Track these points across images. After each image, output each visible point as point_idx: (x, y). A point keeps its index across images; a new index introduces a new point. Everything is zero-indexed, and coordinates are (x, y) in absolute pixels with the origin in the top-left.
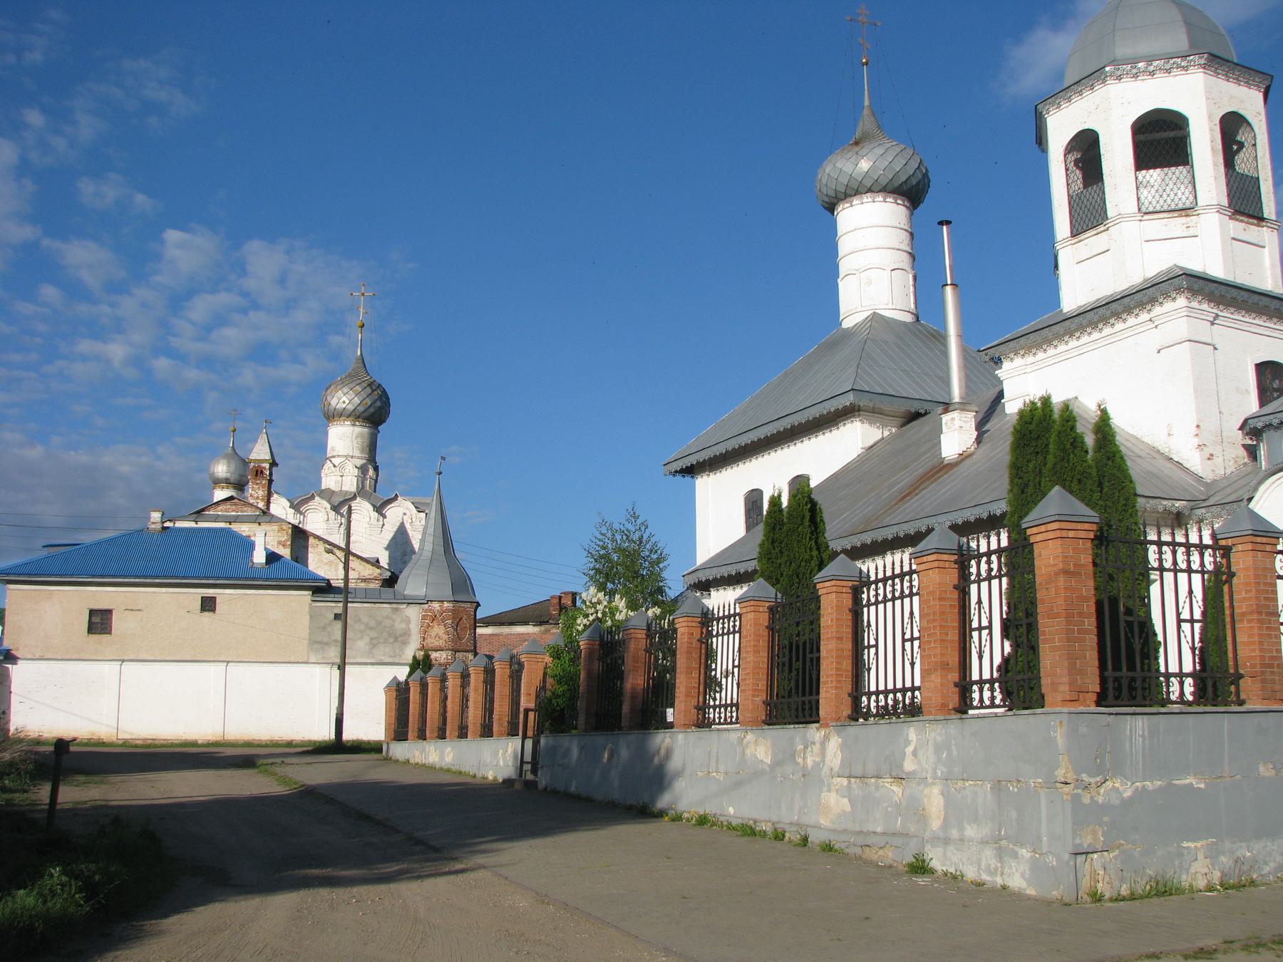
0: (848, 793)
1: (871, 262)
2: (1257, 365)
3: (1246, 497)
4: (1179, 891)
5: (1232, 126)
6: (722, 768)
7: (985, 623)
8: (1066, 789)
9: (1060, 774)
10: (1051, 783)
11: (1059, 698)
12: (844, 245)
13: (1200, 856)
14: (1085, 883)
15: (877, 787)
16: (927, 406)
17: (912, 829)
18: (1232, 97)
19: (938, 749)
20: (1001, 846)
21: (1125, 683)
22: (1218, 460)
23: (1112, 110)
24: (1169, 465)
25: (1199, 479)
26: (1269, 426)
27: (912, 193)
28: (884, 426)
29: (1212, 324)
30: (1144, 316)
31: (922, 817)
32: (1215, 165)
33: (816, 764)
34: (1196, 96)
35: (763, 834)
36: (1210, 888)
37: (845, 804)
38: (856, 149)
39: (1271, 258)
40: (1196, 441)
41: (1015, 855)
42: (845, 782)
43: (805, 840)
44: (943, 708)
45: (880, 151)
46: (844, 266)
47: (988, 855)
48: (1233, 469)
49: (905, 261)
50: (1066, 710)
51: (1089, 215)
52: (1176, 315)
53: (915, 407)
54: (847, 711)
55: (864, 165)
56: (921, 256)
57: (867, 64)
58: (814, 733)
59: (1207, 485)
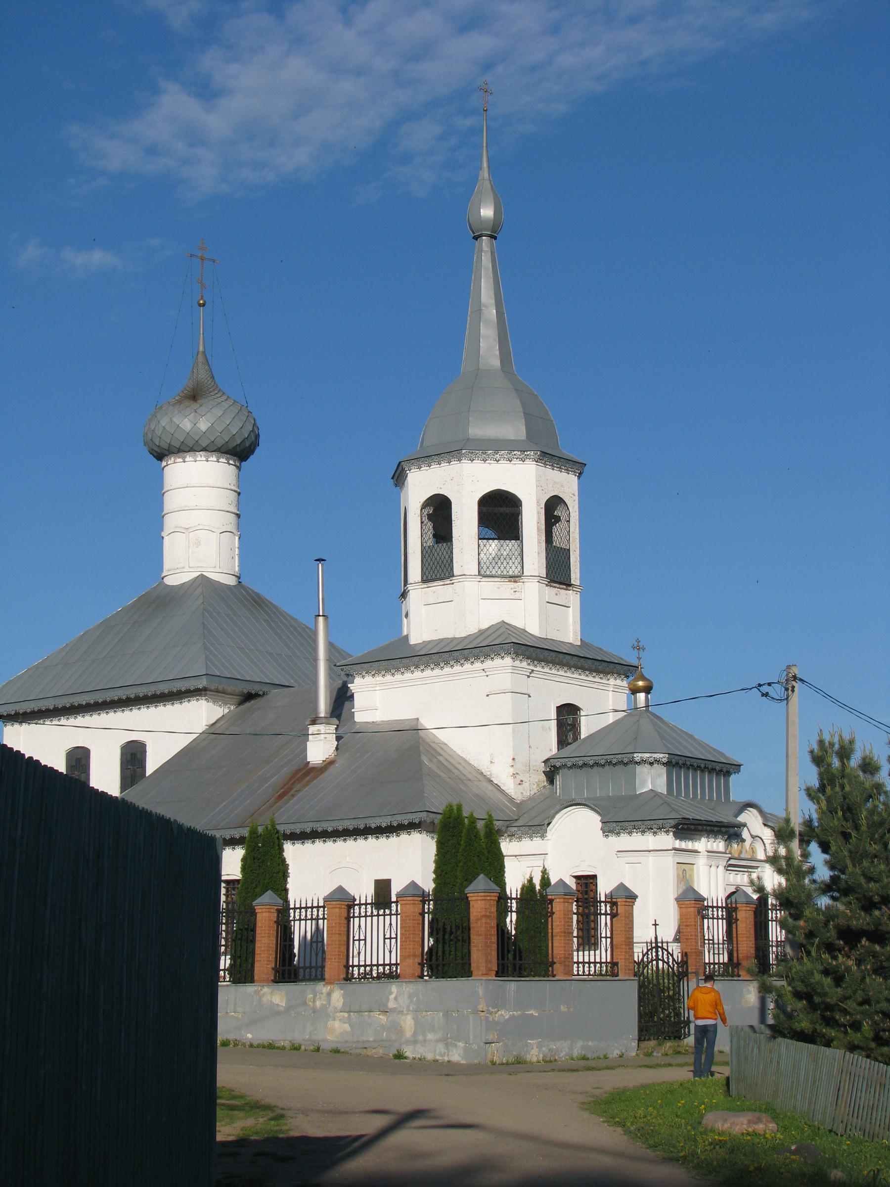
0: (349, 1021)
1: (199, 518)
2: (557, 707)
3: (546, 822)
4: (525, 1062)
5: (553, 508)
6: (240, 1009)
7: (362, 937)
8: (483, 1014)
9: (480, 1007)
10: (476, 1012)
11: (480, 973)
12: (171, 501)
13: (535, 1047)
14: (489, 1056)
15: (369, 1017)
16: (265, 688)
17: (393, 1037)
18: (555, 483)
19: (410, 996)
20: (447, 1042)
21: (517, 966)
22: (526, 785)
23: (466, 483)
24: (490, 787)
25: (511, 800)
26: (564, 766)
27: (240, 452)
28: (225, 704)
29: (529, 677)
30: (478, 665)
31: (400, 1031)
32: (539, 542)
33: (323, 1006)
34: (528, 482)
35: (283, 1048)
36: (538, 1062)
37: (347, 1027)
38: (195, 406)
39: (574, 616)
40: (511, 771)
41: (456, 1046)
42: (346, 1015)
43: (318, 1049)
44: (413, 976)
45: (218, 412)
46: (170, 522)
47: (441, 1047)
48: (535, 791)
49: (229, 522)
50: (484, 978)
51: (438, 568)
52: (503, 670)
53: (254, 689)
54: (343, 976)
55: (203, 425)
56: (247, 515)
57: (204, 305)
58: (322, 988)
59: (519, 805)
